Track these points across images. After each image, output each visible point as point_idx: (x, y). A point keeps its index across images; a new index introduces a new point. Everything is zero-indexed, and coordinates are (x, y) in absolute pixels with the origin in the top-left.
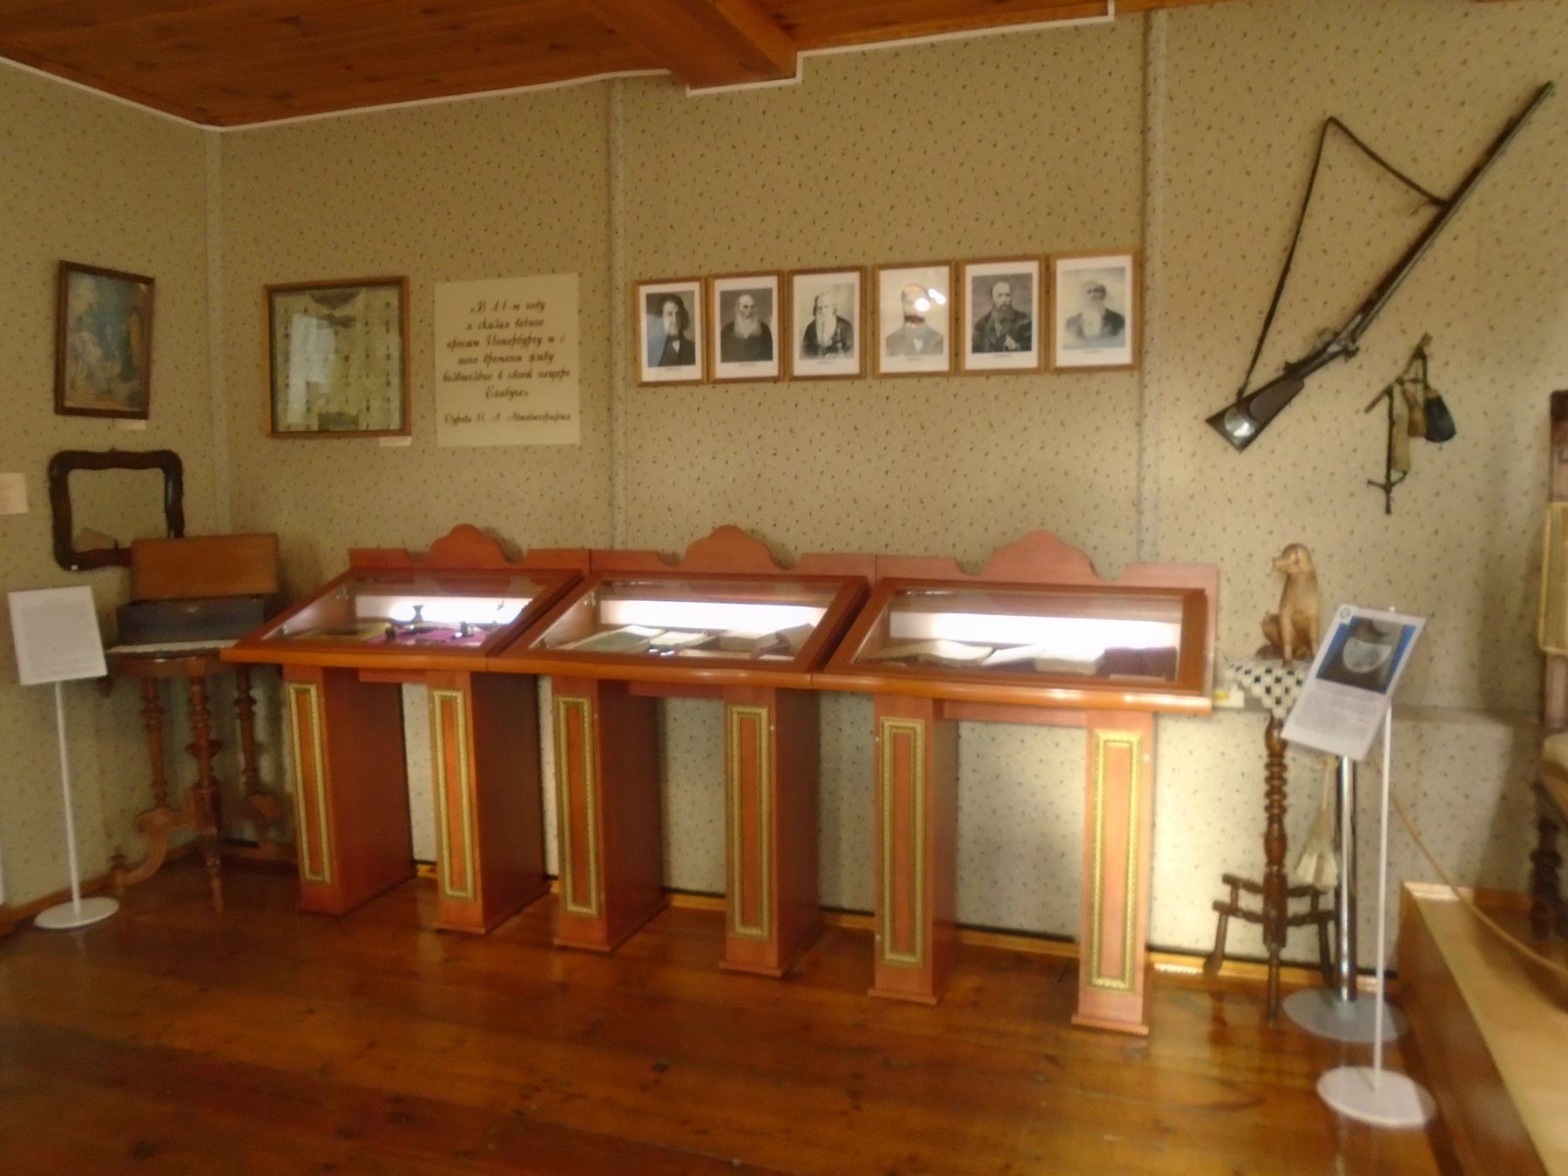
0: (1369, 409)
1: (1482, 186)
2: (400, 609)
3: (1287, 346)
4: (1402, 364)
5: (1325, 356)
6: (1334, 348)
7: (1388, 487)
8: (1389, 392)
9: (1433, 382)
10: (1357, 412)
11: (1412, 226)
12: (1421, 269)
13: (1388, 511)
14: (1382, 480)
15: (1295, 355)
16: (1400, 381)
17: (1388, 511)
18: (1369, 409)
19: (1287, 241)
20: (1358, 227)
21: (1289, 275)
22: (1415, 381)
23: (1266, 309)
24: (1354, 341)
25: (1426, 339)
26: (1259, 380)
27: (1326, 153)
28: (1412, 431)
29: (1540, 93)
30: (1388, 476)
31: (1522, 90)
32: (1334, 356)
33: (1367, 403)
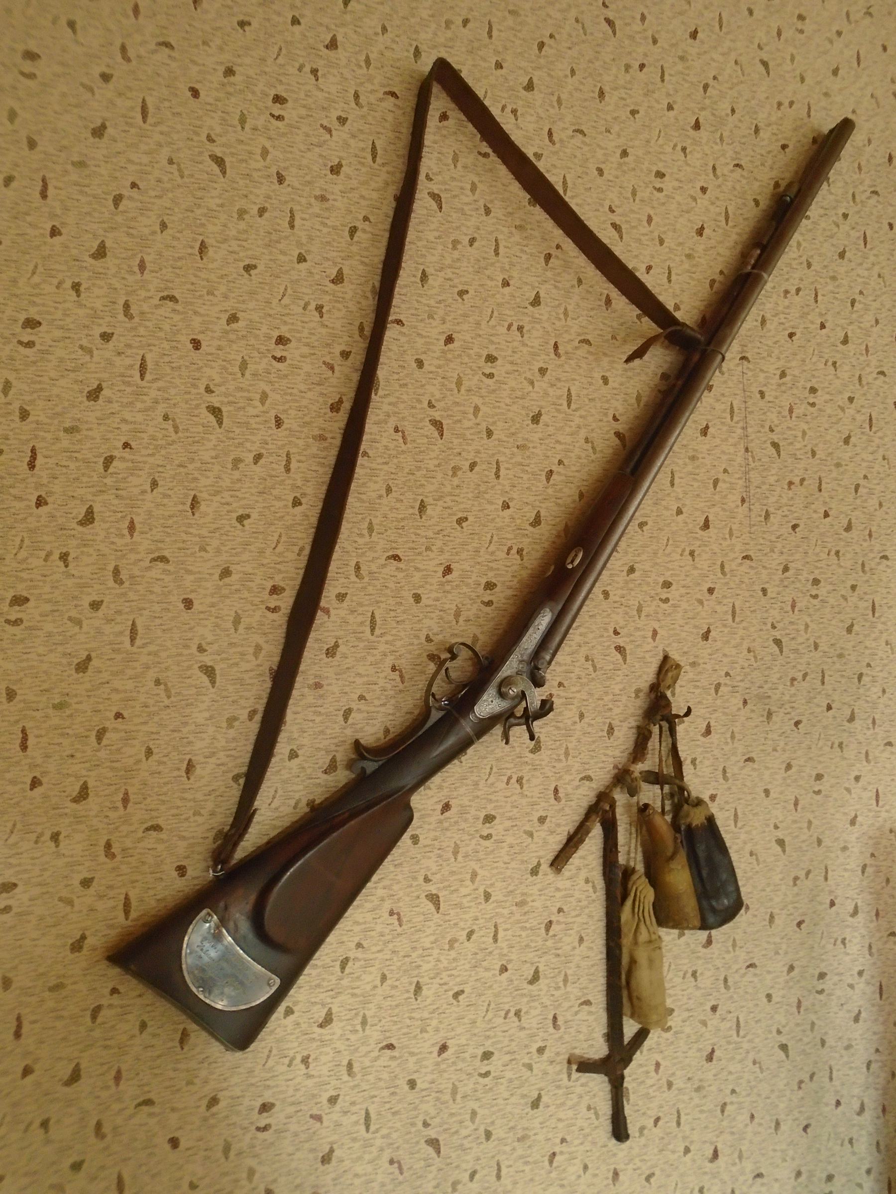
0: (559, 860)
1: (769, 300)
2: (581, 555)
3: (355, 693)
4: (624, 737)
5: (466, 727)
6: (488, 704)
7: (614, 1063)
8: (600, 810)
9: (696, 782)
10: (535, 872)
11: (624, 387)
12: (656, 502)
13: (620, 1131)
14: (599, 1049)
15: (376, 721)
16: (622, 778)
17: (620, 1131)
18: (559, 860)
19: (342, 382)
20: (509, 382)
21: (394, 189)
22: (654, 778)
23: (291, 572)
24: (538, 682)
25: (667, 667)
26: (282, 800)
27: (428, 163)
28: (666, 914)
29: (826, 147)
30: (614, 1032)
31: (765, 170)
32: (484, 727)
33: (556, 842)
